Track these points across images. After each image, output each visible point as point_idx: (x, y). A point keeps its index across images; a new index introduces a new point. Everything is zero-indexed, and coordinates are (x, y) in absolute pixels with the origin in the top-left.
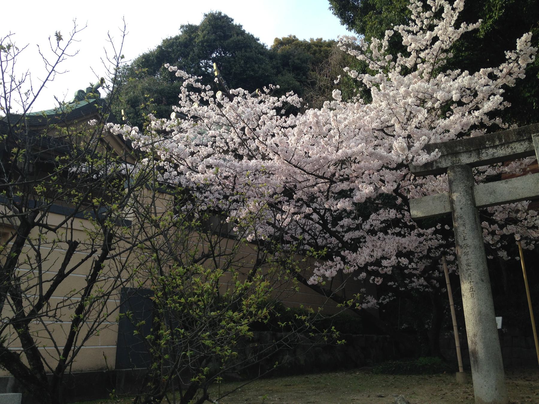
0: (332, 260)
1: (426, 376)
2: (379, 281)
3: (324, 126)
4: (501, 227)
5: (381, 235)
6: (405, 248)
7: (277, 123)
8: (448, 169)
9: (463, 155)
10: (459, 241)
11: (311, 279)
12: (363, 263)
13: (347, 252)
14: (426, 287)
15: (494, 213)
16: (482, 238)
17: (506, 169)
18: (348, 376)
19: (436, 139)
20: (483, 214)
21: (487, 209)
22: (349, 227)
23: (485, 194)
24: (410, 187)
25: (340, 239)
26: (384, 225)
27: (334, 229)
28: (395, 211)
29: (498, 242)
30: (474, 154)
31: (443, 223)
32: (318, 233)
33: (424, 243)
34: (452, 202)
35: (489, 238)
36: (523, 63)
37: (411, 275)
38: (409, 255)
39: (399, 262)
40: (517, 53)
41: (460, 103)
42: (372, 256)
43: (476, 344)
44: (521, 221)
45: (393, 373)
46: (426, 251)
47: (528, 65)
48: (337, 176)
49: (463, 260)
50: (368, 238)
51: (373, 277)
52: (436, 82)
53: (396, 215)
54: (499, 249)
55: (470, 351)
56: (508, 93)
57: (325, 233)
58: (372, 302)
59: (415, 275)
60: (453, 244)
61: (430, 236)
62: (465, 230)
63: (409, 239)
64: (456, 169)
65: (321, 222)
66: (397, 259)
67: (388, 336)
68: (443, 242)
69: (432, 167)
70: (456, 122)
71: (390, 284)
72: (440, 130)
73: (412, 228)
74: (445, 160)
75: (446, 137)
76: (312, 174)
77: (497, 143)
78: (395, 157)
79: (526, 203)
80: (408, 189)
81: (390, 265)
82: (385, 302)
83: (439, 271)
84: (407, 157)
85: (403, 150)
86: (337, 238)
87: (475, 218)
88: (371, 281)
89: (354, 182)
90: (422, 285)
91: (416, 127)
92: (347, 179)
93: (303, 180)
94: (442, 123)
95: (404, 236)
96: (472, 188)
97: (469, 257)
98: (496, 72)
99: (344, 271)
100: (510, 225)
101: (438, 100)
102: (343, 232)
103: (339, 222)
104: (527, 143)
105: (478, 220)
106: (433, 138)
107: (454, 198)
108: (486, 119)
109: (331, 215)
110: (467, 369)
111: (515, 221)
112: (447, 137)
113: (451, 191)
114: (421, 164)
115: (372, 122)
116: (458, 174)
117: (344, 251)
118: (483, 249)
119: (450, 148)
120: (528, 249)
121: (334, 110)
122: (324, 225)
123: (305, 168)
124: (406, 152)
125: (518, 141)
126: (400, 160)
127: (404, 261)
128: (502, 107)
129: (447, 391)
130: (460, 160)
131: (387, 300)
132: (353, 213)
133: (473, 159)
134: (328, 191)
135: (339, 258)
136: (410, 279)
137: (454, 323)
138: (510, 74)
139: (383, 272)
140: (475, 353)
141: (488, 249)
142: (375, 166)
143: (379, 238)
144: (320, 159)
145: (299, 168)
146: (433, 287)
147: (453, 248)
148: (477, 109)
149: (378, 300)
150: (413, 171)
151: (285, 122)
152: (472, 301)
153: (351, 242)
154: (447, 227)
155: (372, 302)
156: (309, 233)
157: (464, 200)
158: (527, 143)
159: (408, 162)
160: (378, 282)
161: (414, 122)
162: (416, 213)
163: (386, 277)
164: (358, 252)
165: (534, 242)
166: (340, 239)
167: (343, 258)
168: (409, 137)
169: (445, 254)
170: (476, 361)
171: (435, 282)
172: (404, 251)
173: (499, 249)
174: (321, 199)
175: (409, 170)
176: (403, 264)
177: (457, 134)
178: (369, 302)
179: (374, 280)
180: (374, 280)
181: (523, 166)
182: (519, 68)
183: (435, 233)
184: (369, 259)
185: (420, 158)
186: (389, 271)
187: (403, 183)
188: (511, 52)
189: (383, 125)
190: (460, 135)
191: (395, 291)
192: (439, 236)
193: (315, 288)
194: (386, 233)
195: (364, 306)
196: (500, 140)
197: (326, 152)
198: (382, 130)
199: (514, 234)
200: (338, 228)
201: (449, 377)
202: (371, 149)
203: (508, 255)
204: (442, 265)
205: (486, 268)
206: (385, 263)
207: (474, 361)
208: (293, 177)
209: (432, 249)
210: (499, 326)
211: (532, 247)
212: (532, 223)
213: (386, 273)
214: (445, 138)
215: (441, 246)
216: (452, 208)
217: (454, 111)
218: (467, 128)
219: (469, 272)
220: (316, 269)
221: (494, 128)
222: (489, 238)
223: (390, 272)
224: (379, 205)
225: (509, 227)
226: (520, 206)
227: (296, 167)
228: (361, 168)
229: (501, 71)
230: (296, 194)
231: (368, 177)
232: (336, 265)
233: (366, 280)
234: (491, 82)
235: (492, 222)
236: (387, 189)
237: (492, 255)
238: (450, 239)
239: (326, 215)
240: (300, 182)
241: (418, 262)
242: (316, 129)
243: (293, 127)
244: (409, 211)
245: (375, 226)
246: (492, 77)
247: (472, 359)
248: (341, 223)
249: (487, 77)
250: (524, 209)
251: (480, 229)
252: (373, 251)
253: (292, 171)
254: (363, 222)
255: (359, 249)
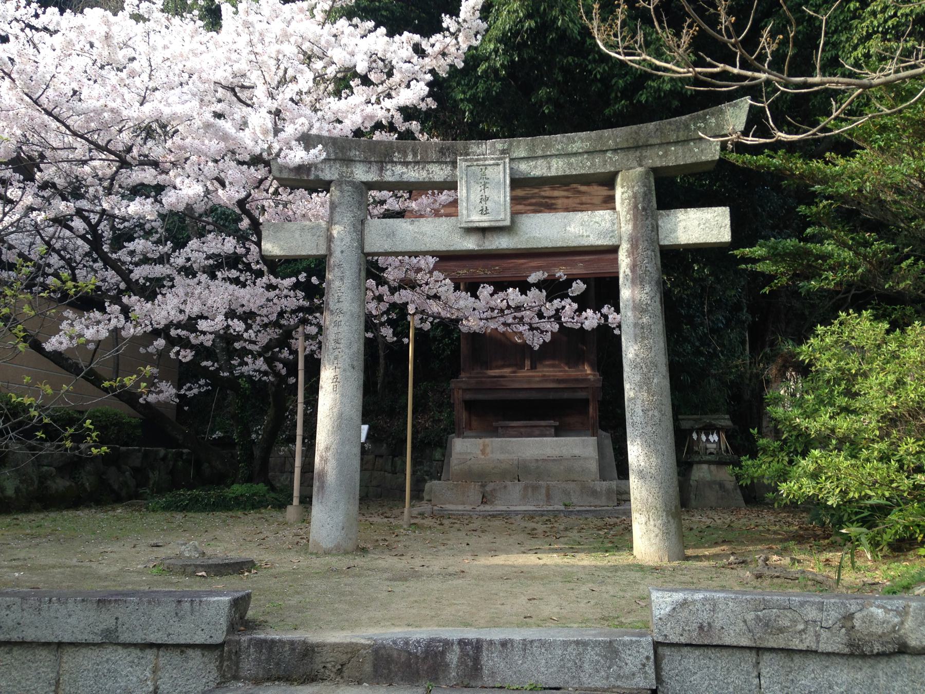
0: (103, 310)
1: (239, 513)
2: (187, 356)
3: (121, 49)
4: (393, 290)
5: (204, 277)
6: (243, 306)
7: (18, 15)
8: (332, 184)
9: (358, 165)
10: (331, 303)
11: (54, 340)
12: (163, 322)
13: (134, 298)
14: (265, 373)
15: (387, 268)
16: (364, 303)
17: (414, 205)
18: (101, 515)
19: (321, 129)
20: (372, 269)
21: (377, 261)
22: (145, 255)
23: (383, 236)
24: (266, 203)
25: (125, 275)
26: (211, 262)
27: (114, 256)
28: (235, 241)
29: (384, 313)
30: (374, 168)
31: (309, 273)
32: (78, 258)
33: (275, 301)
34: (330, 239)
35: (372, 307)
36: (464, 43)
37: (244, 352)
38: (248, 317)
39: (228, 326)
40: (458, 23)
41: (366, 81)
42: (181, 311)
43: (326, 461)
44: (421, 286)
45: (184, 509)
46: (275, 315)
47: (470, 48)
48: (136, 153)
49: (331, 333)
50: (178, 279)
51: (177, 348)
52: (334, 31)
53: (235, 247)
54: (382, 324)
55: (315, 471)
56: (437, 86)
57: (95, 261)
58: (167, 392)
59: (251, 352)
60: (319, 309)
61: (286, 292)
62: (342, 287)
63: (251, 291)
64: (344, 186)
65: (89, 236)
66: (226, 320)
67: (185, 451)
68: (305, 303)
69: (308, 175)
70: (355, 110)
71: (204, 364)
72: (329, 116)
73: (260, 274)
74: (331, 167)
75: (338, 129)
76: (82, 137)
77: (410, 158)
78: (249, 143)
79: (431, 261)
80: (263, 206)
81: (211, 329)
82: (190, 394)
83: (290, 349)
84: (270, 147)
85: (265, 132)
86: (119, 271)
87: (360, 270)
88: (172, 355)
89: (167, 173)
90: (259, 371)
91: (292, 100)
92: (155, 164)
93: (61, 145)
94: (333, 105)
95: (244, 285)
96: (363, 222)
97: (341, 330)
98: (425, 44)
99: (123, 333)
100: (406, 289)
101: (333, 63)
102: (131, 263)
103: (126, 244)
104: (449, 168)
105: (363, 274)
106: (317, 125)
107: (335, 233)
108: (398, 117)
109: (113, 228)
110: (306, 501)
111: (411, 285)
112: (337, 131)
113: (331, 222)
114: (292, 166)
115: (217, 67)
116: (346, 194)
117: (130, 297)
118: (363, 319)
119: (343, 149)
120: (421, 329)
121: (146, 20)
122: (95, 240)
123: (69, 122)
124: (270, 138)
125: (438, 162)
126: (257, 151)
127: (238, 326)
128: (423, 106)
129: (268, 534)
130: (352, 173)
131: (195, 391)
132: (157, 232)
133: (372, 177)
134: (112, 179)
135: (117, 308)
136: (241, 358)
137: (299, 431)
138: (444, 54)
139: (198, 342)
140: (322, 474)
141: (370, 323)
142: (212, 150)
143: (199, 283)
144: (103, 111)
145: (57, 118)
146: (277, 374)
147: (318, 315)
148: (389, 96)
149: (179, 388)
150: (278, 175)
151: (37, 16)
152: (335, 398)
153: (144, 284)
154: (314, 280)
155: (167, 392)
156: (60, 255)
157: (348, 239)
158: (449, 168)
159: (271, 157)
160: (185, 357)
161: (290, 91)
162: (271, 247)
163: (202, 352)
164: (156, 302)
165: (431, 319)
166: (125, 275)
167: (126, 311)
168: (277, 113)
169: (304, 322)
170: (322, 487)
171: (281, 366)
172: (240, 311)
173: (382, 324)
174: (97, 191)
175: (270, 172)
176: (235, 330)
177: (354, 129)
178: (161, 392)
179: (178, 353)
180: (178, 353)
181: (437, 206)
182: (458, 49)
183: (296, 286)
184: (176, 317)
185: (292, 154)
186: (208, 340)
187: (255, 194)
188: (451, 17)
189: (235, 81)
190: (358, 133)
191: (213, 377)
192: (301, 294)
193: (57, 357)
194: (213, 277)
195: (152, 398)
196: (415, 155)
197: (114, 100)
198: (233, 90)
199: (407, 303)
200: (122, 255)
201: (274, 513)
202: (208, 117)
203: (394, 334)
204: (297, 339)
205: (362, 348)
206: (203, 325)
207: (318, 487)
208: (39, 135)
209: (286, 312)
210: (363, 439)
211: (427, 326)
212: (435, 291)
213: (202, 343)
214: (335, 132)
215: (300, 309)
216: (329, 248)
217: (355, 91)
218: (369, 125)
219: (336, 353)
220: (65, 322)
221: (408, 135)
222: (372, 307)
223: (210, 343)
224: (207, 227)
225: (403, 292)
226: (422, 264)
227: (49, 114)
228: (181, 148)
229: (433, 46)
230: (40, 170)
231: (196, 168)
232: (109, 320)
233: (163, 354)
234: (415, 59)
235: (381, 281)
236: (227, 197)
237: (372, 332)
238: (315, 300)
239: (102, 225)
240: (53, 148)
241: (259, 331)
242: (103, 48)
243: (53, 33)
244: (258, 244)
245: (195, 262)
246: (419, 51)
247: (316, 484)
248: (131, 246)
249: (411, 49)
250: (428, 267)
251: (363, 289)
252: (185, 302)
253: (38, 121)
254: (174, 251)
255: (159, 297)
